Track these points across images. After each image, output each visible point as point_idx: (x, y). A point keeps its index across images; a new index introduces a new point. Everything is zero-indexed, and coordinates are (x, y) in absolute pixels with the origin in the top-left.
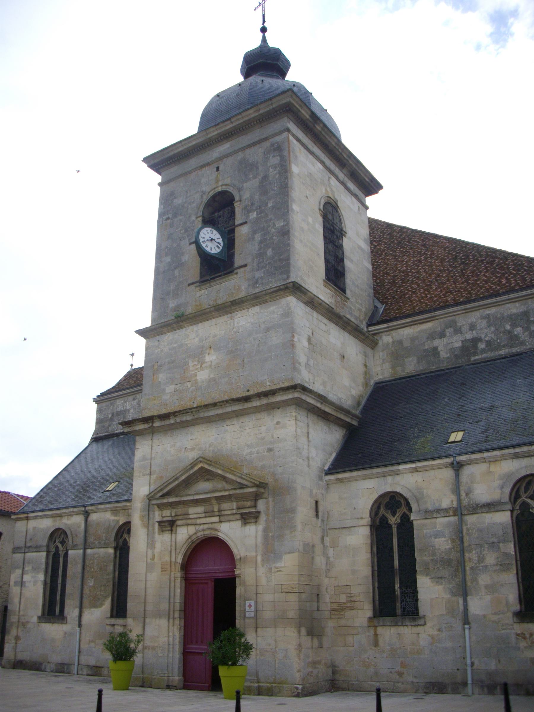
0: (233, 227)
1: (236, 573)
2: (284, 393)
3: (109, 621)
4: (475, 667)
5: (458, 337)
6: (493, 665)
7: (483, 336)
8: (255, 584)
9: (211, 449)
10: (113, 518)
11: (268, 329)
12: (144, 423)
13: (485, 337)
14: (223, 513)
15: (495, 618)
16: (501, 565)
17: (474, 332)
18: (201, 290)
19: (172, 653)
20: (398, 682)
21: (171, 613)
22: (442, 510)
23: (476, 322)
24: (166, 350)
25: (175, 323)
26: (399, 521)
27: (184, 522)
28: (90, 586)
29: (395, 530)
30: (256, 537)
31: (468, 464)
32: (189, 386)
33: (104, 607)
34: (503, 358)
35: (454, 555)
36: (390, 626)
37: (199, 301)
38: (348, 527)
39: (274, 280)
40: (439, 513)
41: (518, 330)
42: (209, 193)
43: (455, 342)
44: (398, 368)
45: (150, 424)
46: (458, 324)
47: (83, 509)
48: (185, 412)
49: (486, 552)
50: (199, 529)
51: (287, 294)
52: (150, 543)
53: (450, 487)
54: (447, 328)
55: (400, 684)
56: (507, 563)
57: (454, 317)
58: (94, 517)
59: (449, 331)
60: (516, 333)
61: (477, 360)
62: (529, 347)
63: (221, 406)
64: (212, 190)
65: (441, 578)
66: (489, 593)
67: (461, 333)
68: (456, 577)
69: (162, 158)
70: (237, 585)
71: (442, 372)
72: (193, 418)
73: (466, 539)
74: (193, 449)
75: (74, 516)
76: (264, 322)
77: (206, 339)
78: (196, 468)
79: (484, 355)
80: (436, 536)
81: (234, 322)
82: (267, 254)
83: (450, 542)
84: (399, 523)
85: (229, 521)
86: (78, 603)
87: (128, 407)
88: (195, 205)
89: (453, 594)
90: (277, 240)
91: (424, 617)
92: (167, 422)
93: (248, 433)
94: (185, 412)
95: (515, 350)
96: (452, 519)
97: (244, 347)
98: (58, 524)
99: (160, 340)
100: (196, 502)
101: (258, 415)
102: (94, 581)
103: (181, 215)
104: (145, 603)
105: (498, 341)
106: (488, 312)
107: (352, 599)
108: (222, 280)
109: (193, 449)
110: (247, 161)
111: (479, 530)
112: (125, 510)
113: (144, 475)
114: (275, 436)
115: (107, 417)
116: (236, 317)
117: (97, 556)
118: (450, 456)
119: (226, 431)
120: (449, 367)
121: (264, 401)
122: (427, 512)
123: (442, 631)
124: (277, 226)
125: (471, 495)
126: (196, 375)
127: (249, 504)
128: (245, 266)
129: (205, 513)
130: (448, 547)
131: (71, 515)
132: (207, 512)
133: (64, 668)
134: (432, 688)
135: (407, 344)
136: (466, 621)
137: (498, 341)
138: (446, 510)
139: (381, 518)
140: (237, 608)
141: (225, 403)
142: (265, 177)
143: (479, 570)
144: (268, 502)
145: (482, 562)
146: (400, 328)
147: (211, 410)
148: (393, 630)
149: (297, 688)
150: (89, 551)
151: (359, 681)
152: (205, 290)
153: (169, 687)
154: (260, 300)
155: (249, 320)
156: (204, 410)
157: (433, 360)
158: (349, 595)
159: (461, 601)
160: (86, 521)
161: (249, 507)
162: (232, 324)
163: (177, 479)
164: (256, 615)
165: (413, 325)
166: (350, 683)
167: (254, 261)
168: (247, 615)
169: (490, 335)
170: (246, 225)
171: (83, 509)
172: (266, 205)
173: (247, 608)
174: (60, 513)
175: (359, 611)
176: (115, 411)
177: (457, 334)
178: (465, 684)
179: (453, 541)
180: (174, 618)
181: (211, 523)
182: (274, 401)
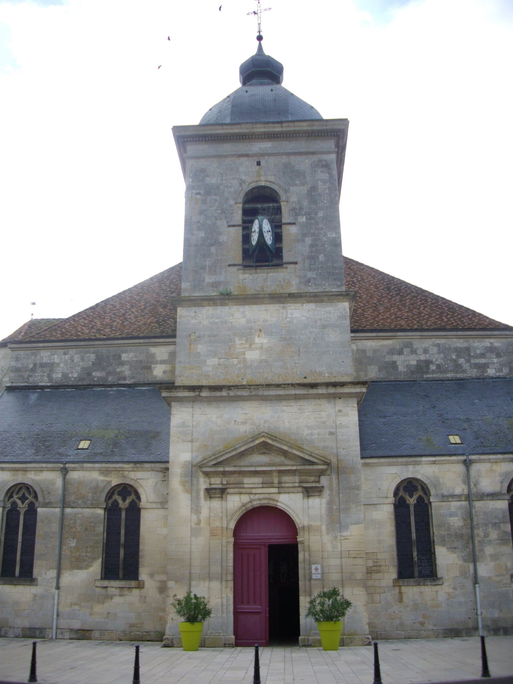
0: (280, 224)
1: (298, 540)
2: (353, 386)
3: (99, 583)
4: (483, 615)
5: (414, 357)
6: (496, 614)
7: (434, 360)
8: (321, 550)
9: (266, 425)
10: (101, 478)
11: (324, 327)
12: (188, 391)
13: (436, 361)
14: (283, 485)
15: (498, 579)
16: (501, 540)
17: (427, 355)
18: (244, 273)
19: (225, 613)
20: (421, 630)
21: (224, 576)
22: (456, 495)
23: (428, 348)
24: (205, 322)
25: (220, 299)
26: (416, 502)
27: (237, 490)
28: (71, 547)
29: (412, 509)
30: (320, 509)
31: (476, 462)
32: (235, 363)
33: (91, 569)
34: (449, 380)
35: (466, 531)
36: (413, 586)
37: (243, 284)
38: (374, 504)
39: (327, 284)
40: (454, 498)
41: (461, 361)
42: (250, 184)
43: (412, 360)
44: (361, 373)
45: (197, 393)
46: (414, 346)
47: (62, 466)
48: (242, 387)
49: (490, 530)
50: (254, 498)
51: (345, 300)
52: (194, 508)
53: (462, 478)
54: (405, 348)
55: (422, 632)
56: (506, 538)
57: (411, 340)
58: (74, 475)
59: (406, 351)
60: (460, 362)
61: (428, 378)
62: (469, 375)
63: (284, 388)
64: (255, 182)
65: (455, 548)
66: (493, 561)
67: (416, 354)
68: (467, 548)
69: (197, 133)
70: (299, 551)
71: (400, 383)
72: (251, 394)
73: (475, 519)
74: (244, 423)
75: (45, 472)
76: (321, 319)
77: (255, 322)
78: (257, 442)
79: (435, 375)
80: (451, 516)
81: (287, 312)
82: (319, 259)
83: (462, 520)
84: (416, 504)
85: (289, 493)
86: (55, 564)
87: (57, 360)
88: (232, 189)
89: (465, 561)
90: (329, 249)
91: (442, 578)
92: (218, 394)
93: (308, 416)
94: (242, 387)
95: (459, 376)
96: (464, 503)
97: (299, 337)
98: (21, 479)
99: (197, 311)
100: (256, 473)
101: (318, 402)
102: (77, 543)
103: (215, 195)
104: (190, 566)
105: (446, 366)
106: (439, 342)
107: (378, 564)
108: (269, 270)
109: (244, 423)
110: (293, 166)
111: (485, 513)
112: (119, 471)
113: (184, 441)
114: (338, 422)
115: (26, 367)
116: (289, 308)
117: (80, 516)
118: (463, 455)
119: (282, 411)
120: (406, 380)
121: (332, 390)
122: (443, 496)
123: (456, 589)
124: (328, 236)
125: (478, 486)
126: (244, 354)
127: (312, 479)
128: (296, 263)
129: (263, 484)
130: (461, 524)
131: (41, 470)
132: (265, 484)
133: (35, 632)
134: (449, 633)
135: (369, 354)
136: (476, 581)
137: (446, 366)
138: (459, 496)
139: (400, 498)
140: (301, 572)
141: (290, 386)
142: (314, 188)
143: (485, 543)
144: (331, 479)
145: (487, 537)
146: (364, 339)
147: (273, 390)
148: (416, 589)
149: (368, 638)
150: (68, 510)
151: (386, 631)
152: (250, 275)
153: (225, 645)
154: (318, 299)
155: (304, 314)
156: (265, 389)
157: (392, 371)
158: (375, 560)
159: (471, 566)
160: (64, 479)
161: (313, 482)
162: (285, 314)
163: (235, 449)
164: (322, 577)
165: (376, 339)
166: (379, 633)
167: (305, 261)
168: (314, 577)
169: (440, 360)
170: (294, 226)
171: (62, 466)
172: (316, 214)
173: (313, 571)
174: (26, 468)
175: (385, 574)
176: (38, 362)
177: (413, 354)
178: (476, 629)
179: (464, 520)
180: (227, 581)
181: (269, 493)
182: (342, 391)
